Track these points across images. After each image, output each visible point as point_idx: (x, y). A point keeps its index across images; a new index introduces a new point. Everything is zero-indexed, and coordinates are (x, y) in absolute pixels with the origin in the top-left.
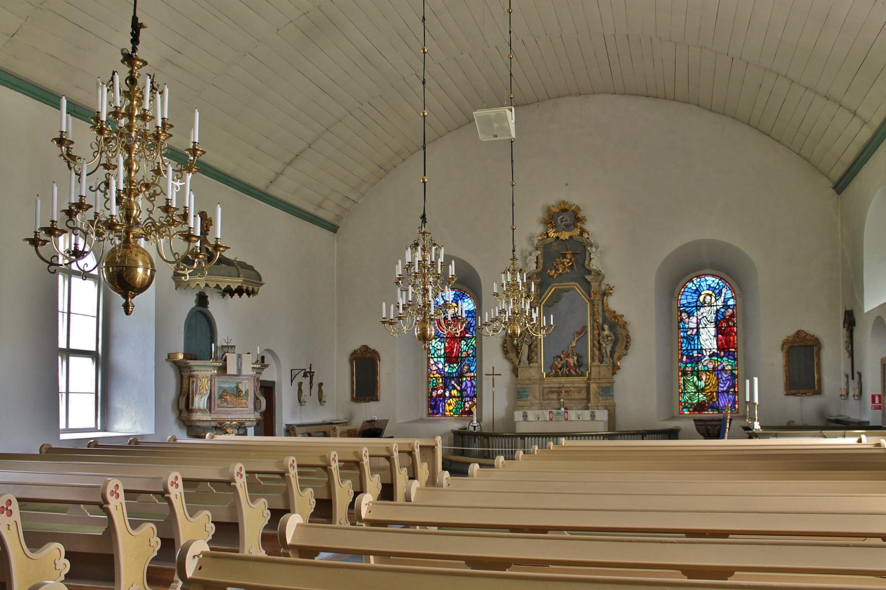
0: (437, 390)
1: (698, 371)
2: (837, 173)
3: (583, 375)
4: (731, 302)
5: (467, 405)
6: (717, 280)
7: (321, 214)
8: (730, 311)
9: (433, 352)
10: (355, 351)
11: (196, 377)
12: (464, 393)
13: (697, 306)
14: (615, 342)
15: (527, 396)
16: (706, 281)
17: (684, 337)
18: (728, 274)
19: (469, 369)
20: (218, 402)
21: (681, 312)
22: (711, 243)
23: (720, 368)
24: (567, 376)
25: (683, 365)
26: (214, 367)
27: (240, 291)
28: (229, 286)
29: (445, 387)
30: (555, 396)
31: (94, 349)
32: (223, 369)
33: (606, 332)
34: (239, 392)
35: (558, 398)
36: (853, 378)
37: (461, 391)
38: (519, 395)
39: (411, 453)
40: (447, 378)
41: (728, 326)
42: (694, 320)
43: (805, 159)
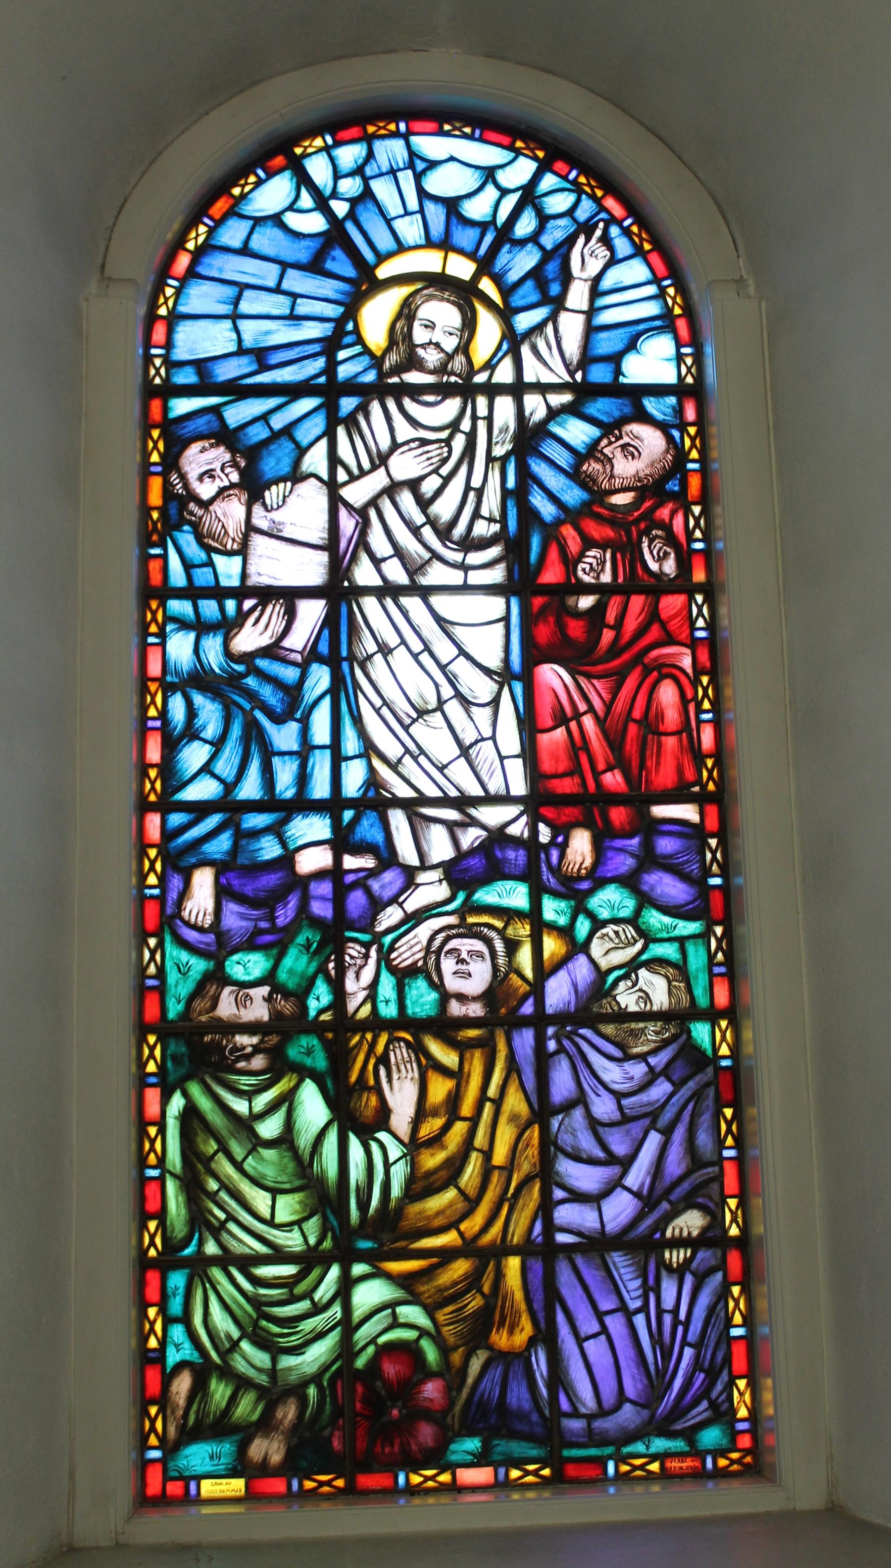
1: (340, 1028)
4: (653, 363)
6: (522, 170)
8: (651, 441)
16: (420, 166)
17: (199, 679)
23: (559, 992)
25: (184, 969)
42: (303, 510)
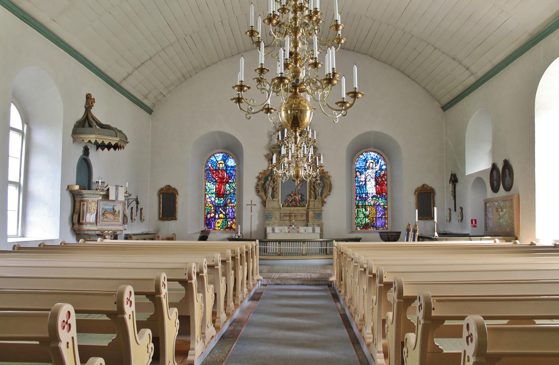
0: (210, 214)
1: (365, 205)
2: (445, 100)
3: (304, 206)
4: (384, 167)
5: (229, 223)
6: (376, 155)
7: (145, 102)
9: (208, 190)
10: (162, 189)
11: (87, 201)
12: (228, 216)
13: (365, 169)
14: (323, 188)
15: (271, 218)
17: (358, 186)
18: (382, 151)
19: (231, 201)
20: (101, 218)
21: (356, 171)
22: (376, 133)
24: (295, 206)
26: (100, 195)
27: (109, 146)
28: (110, 143)
29: (216, 212)
30: (287, 218)
31: (18, 181)
32: (106, 197)
33: (319, 182)
34: (114, 211)
35: (288, 220)
36: (455, 210)
37: (226, 215)
38: (266, 217)
40: (217, 207)
41: (382, 180)
42: (363, 176)
43: (427, 91)
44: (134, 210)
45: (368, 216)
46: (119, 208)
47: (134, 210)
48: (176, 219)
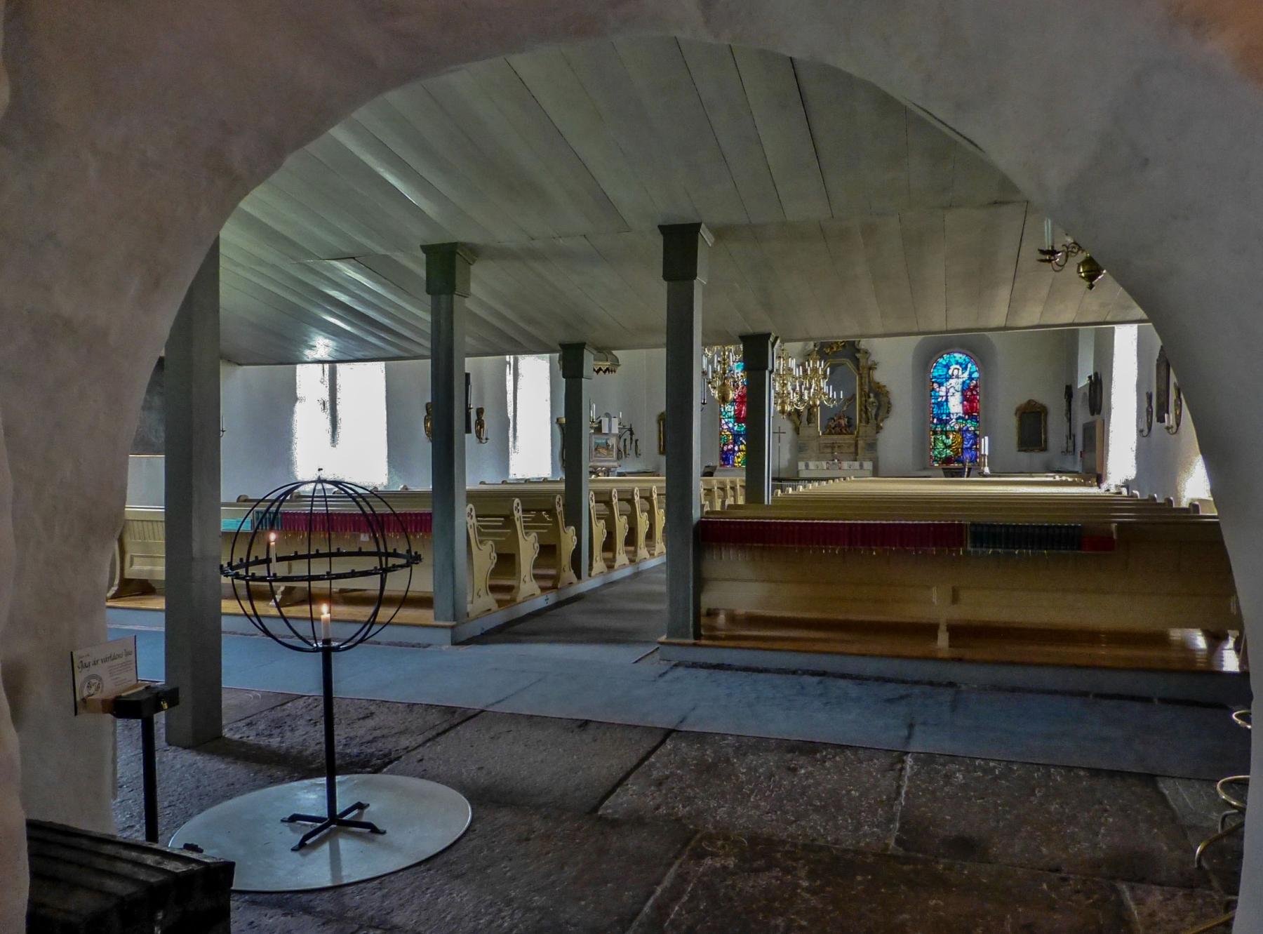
3: (852, 433)
4: (976, 375)
14: (878, 408)
29: (735, 443)
30: (829, 450)
33: (872, 399)
35: (831, 452)
38: (800, 449)
39: (631, 501)
42: (943, 389)
44: (628, 442)
45: (950, 447)
46: (613, 441)
47: (628, 442)
48: (233, 864)
